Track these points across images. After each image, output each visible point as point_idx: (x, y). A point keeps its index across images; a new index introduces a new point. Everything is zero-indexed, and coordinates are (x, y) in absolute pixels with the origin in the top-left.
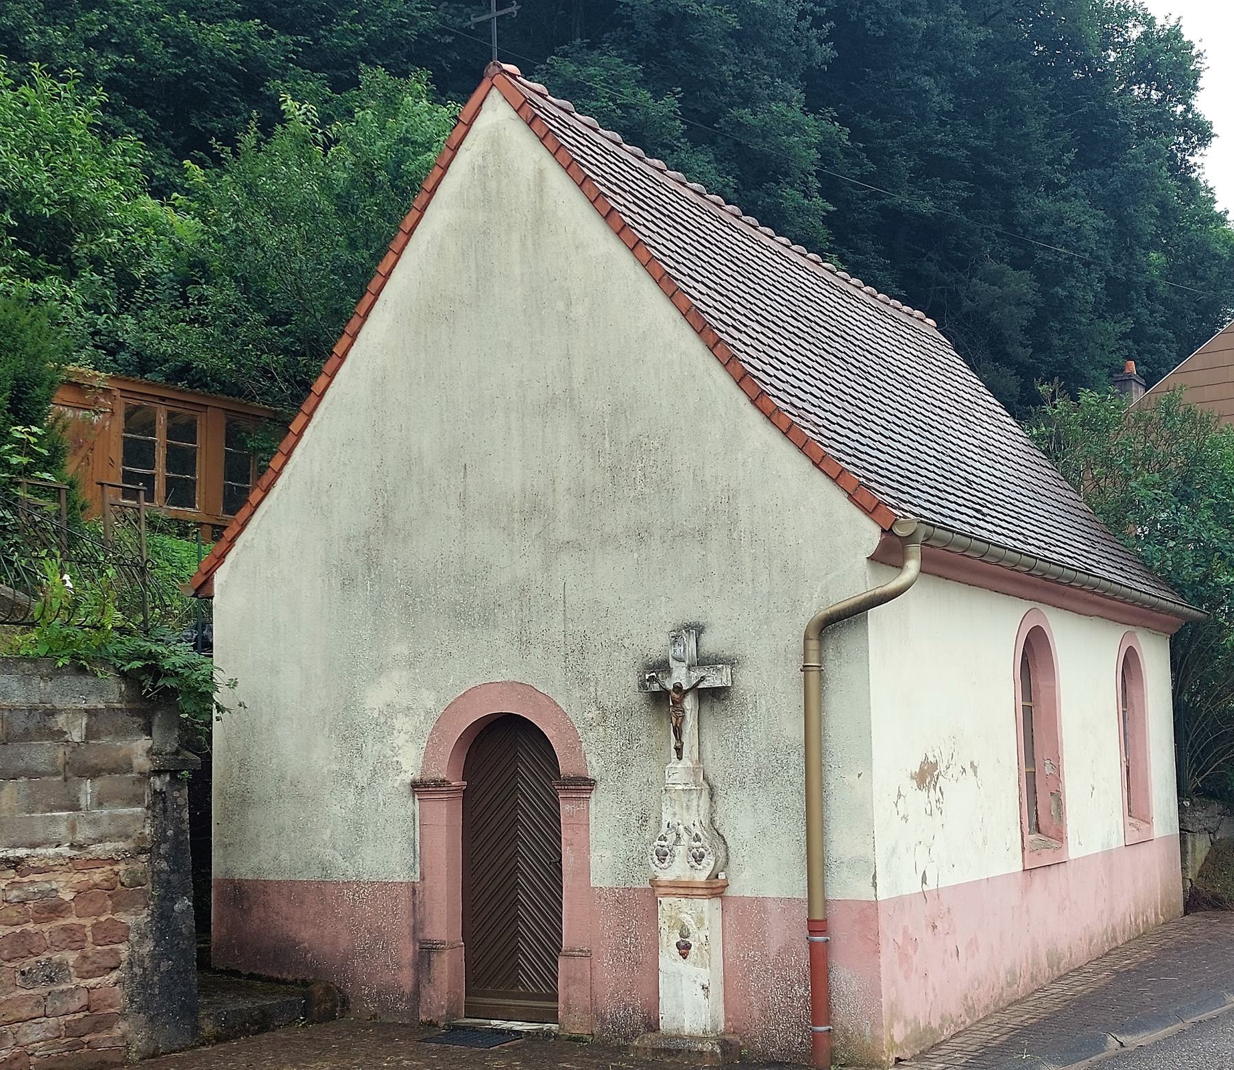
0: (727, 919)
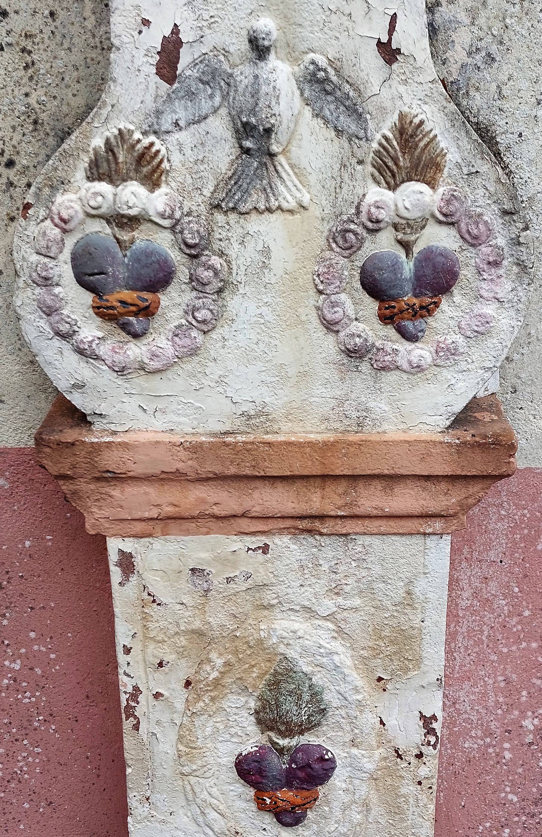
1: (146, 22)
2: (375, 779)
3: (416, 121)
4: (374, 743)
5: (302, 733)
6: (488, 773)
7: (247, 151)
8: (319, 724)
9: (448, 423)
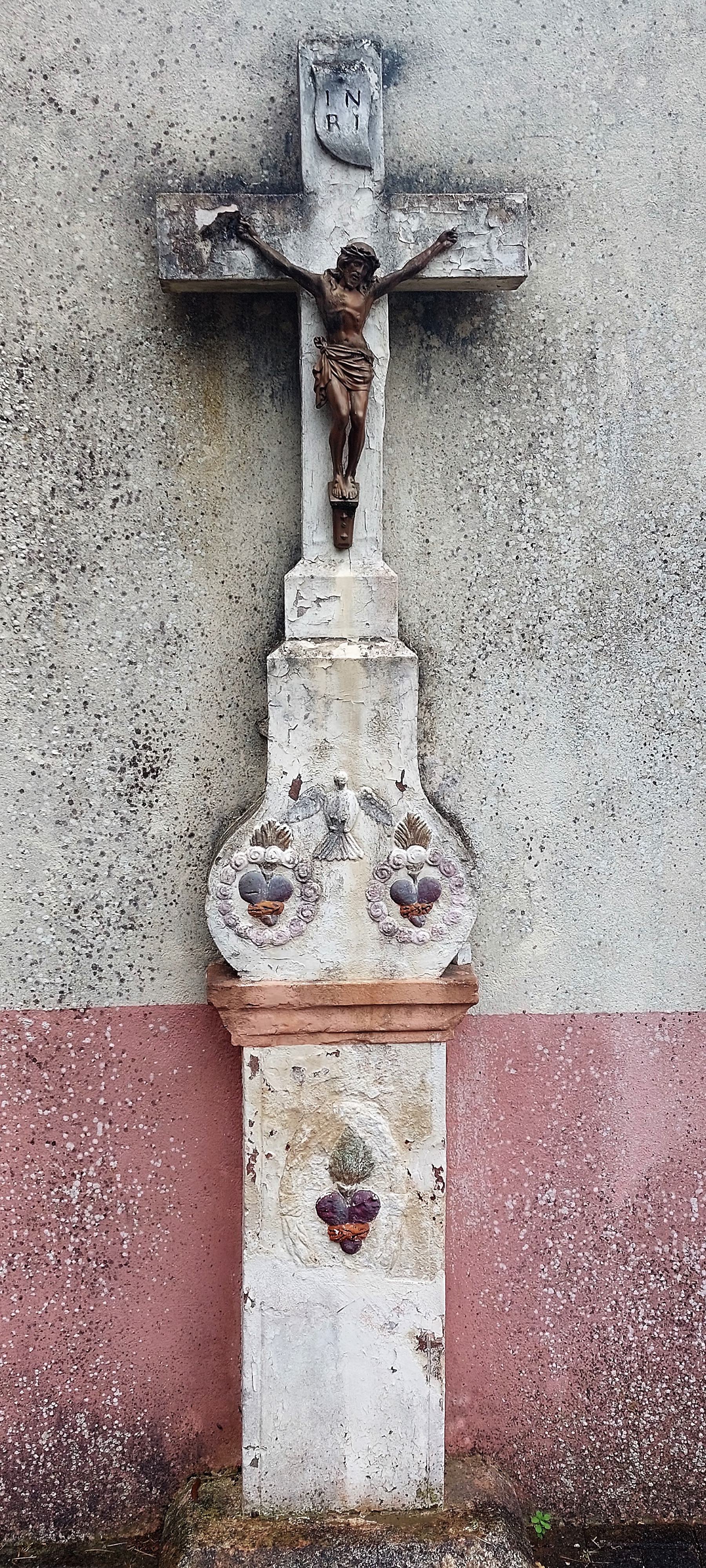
0: (460, 1090)
1: (285, 773)
2: (406, 1216)
3: (416, 817)
4: (404, 1188)
5: (358, 1182)
6: (485, 1246)
7: (333, 831)
8: (369, 1175)
9: (441, 973)
